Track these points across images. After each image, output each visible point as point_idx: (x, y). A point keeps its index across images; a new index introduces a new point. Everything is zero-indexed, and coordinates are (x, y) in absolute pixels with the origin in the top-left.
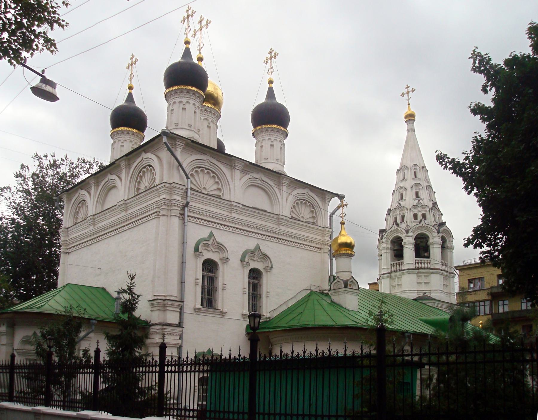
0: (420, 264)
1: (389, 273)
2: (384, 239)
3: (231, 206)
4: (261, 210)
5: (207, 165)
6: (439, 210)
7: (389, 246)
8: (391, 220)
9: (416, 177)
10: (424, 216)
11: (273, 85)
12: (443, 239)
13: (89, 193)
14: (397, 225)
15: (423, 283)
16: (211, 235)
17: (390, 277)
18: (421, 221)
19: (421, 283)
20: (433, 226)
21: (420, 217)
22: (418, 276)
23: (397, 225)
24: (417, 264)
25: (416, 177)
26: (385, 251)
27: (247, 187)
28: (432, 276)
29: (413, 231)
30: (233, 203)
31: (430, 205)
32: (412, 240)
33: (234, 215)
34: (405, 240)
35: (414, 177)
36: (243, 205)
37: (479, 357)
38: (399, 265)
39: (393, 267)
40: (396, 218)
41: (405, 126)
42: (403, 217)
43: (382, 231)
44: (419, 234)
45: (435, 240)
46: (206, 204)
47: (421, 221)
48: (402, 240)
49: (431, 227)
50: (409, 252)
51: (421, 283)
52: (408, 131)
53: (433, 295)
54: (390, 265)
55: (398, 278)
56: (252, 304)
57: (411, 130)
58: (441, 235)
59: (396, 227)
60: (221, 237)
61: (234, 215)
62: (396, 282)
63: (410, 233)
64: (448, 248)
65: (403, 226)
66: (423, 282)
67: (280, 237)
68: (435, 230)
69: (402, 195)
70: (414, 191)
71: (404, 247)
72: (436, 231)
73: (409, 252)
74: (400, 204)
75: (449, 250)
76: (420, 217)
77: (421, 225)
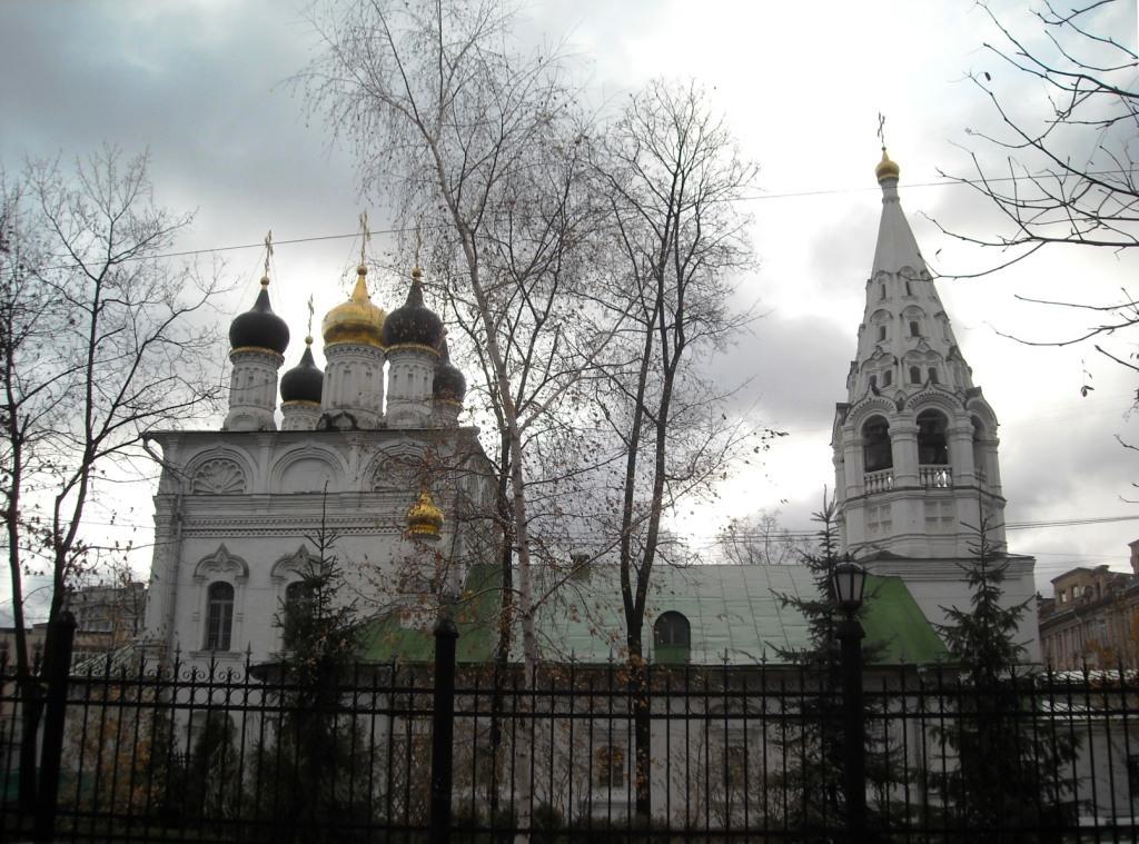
0: (874, 483)
1: (863, 497)
2: (848, 424)
3: (252, 501)
4: (311, 493)
5: (221, 454)
6: (964, 363)
7: (859, 436)
8: (862, 381)
9: (909, 293)
10: (933, 373)
11: (312, 346)
12: (974, 420)
13: (308, 357)
14: (877, 392)
15: (939, 521)
16: (223, 549)
17: (866, 505)
18: (926, 386)
19: (876, 525)
20: (955, 395)
21: (924, 376)
22: (926, 504)
23: (877, 392)
24: (923, 477)
25: (909, 293)
26: (851, 449)
27: (284, 473)
28: (960, 502)
29: (915, 405)
30: (254, 497)
31: (945, 351)
32: (912, 424)
33: (260, 512)
34: (895, 425)
35: (906, 294)
36: (271, 495)
37: (115, 694)
38: (877, 481)
39: (869, 485)
40: (873, 380)
41: (879, 194)
42: (888, 376)
43: (841, 408)
44: (865, 424)
45: (958, 422)
46: (215, 509)
47: (926, 386)
48: (888, 427)
49: (950, 396)
50: (904, 451)
51: (876, 525)
52: (885, 201)
53: (894, 549)
54: (862, 479)
55: (883, 508)
56: (218, 631)
57: (891, 200)
58: (970, 413)
59: (874, 398)
60: (236, 548)
61: (260, 512)
62: (878, 517)
63: (906, 411)
64: (985, 443)
65: (889, 394)
66: (939, 515)
67: (349, 525)
68: (958, 402)
69: (883, 330)
70: (907, 323)
71: (893, 440)
72: (961, 406)
73: (904, 451)
74: (881, 349)
75: (987, 448)
76: (924, 376)
77: (926, 391)
